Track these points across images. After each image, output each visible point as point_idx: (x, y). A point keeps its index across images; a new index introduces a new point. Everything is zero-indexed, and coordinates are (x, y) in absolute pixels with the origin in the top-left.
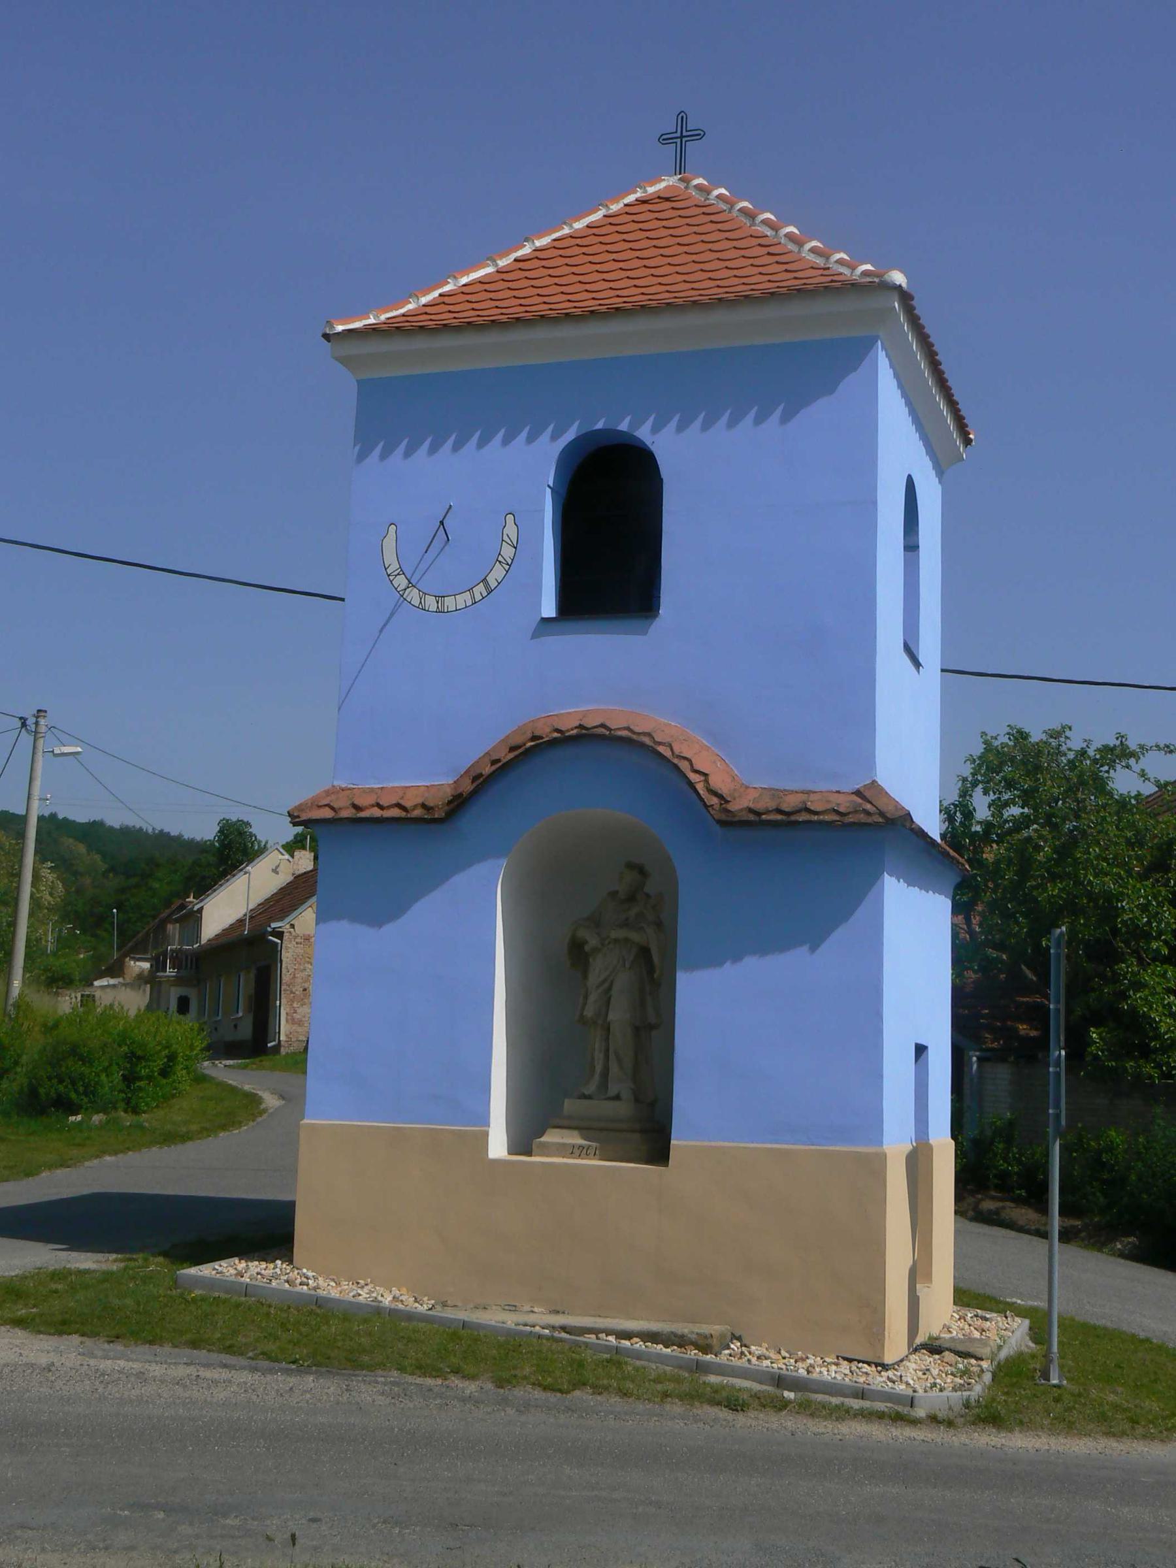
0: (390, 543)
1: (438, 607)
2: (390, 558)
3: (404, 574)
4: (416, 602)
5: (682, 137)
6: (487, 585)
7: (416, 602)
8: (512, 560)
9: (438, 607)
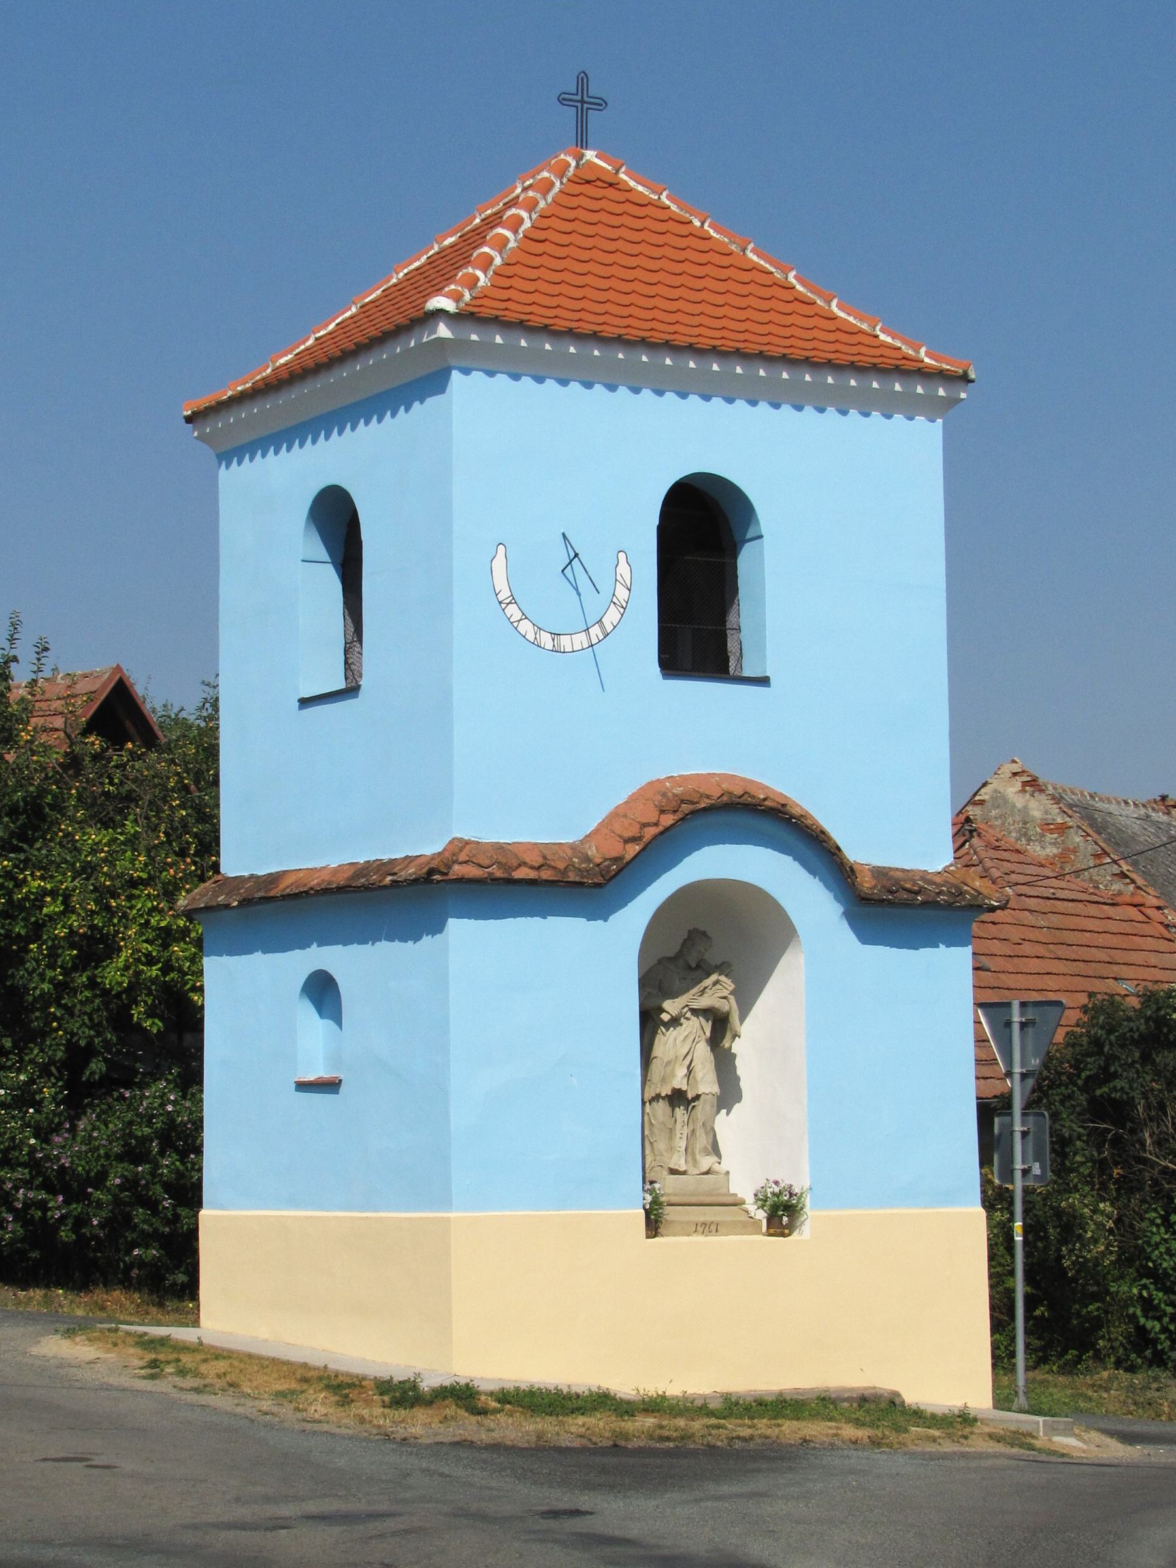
0: (499, 564)
1: (554, 646)
2: (501, 583)
3: (516, 603)
4: (531, 637)
5: (582, 102)
6: (602, 627)
7: (531, 637)
8: (627, 603)
9: (554, 646)
